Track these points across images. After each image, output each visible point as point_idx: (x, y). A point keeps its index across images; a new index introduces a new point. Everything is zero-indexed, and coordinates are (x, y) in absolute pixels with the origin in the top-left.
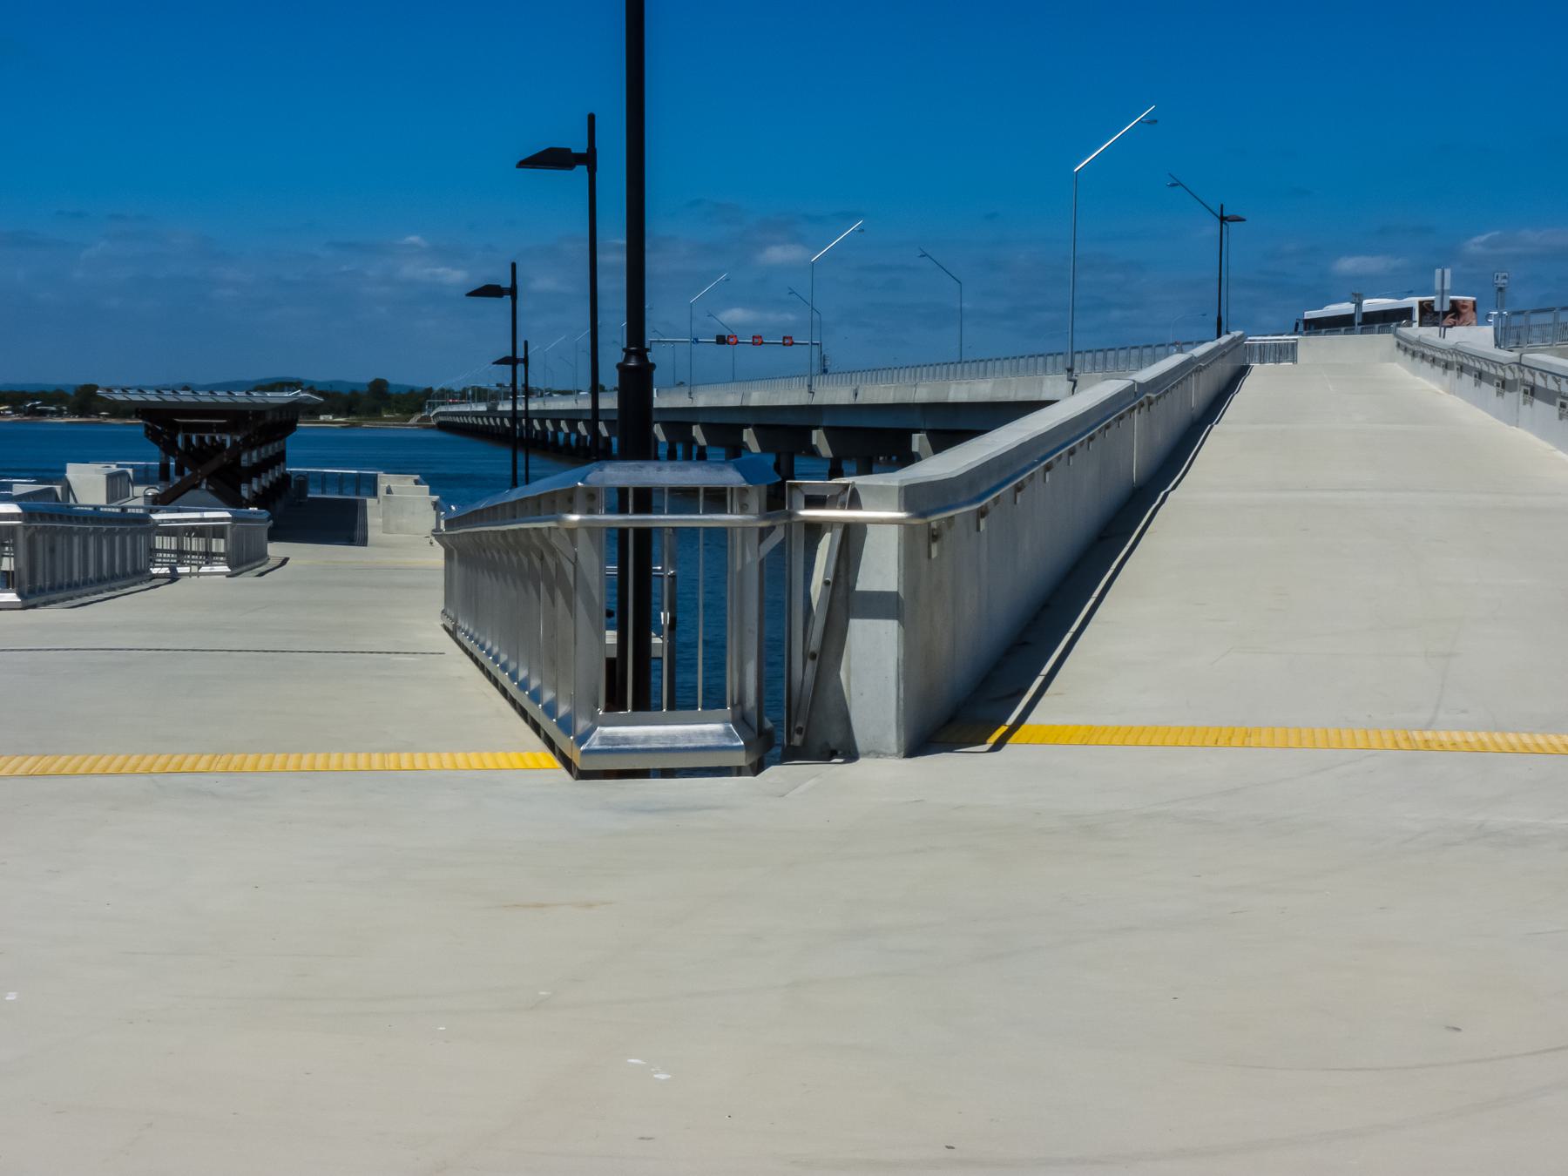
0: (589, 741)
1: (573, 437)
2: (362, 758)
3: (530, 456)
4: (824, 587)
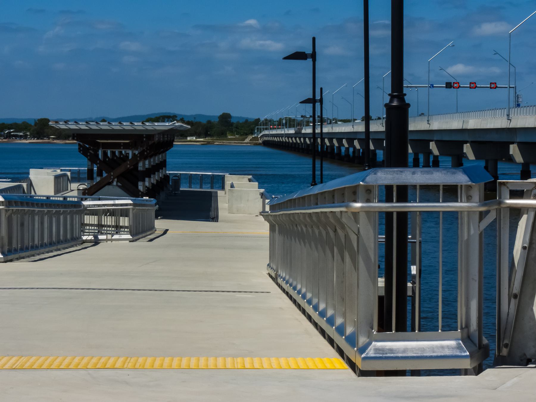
0: (367, 351)
1: (351, 150)
2: (220, 360)
3: (324, 163)
4: (523, 250)
